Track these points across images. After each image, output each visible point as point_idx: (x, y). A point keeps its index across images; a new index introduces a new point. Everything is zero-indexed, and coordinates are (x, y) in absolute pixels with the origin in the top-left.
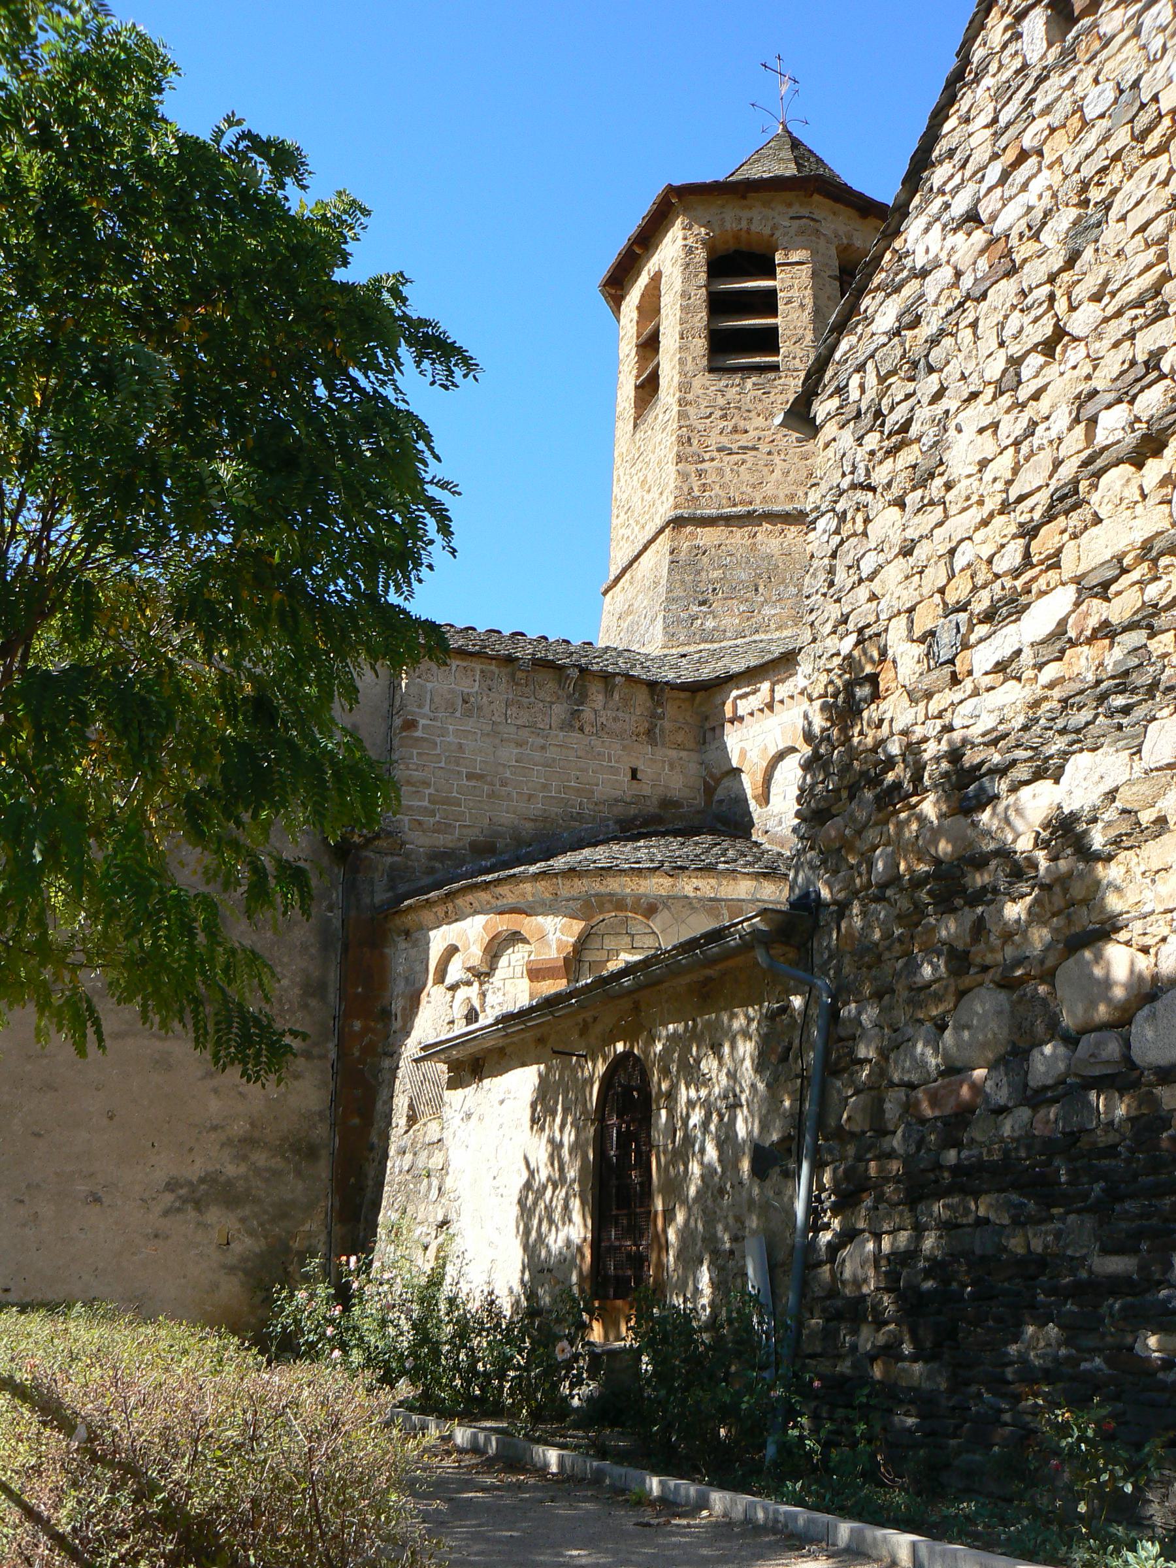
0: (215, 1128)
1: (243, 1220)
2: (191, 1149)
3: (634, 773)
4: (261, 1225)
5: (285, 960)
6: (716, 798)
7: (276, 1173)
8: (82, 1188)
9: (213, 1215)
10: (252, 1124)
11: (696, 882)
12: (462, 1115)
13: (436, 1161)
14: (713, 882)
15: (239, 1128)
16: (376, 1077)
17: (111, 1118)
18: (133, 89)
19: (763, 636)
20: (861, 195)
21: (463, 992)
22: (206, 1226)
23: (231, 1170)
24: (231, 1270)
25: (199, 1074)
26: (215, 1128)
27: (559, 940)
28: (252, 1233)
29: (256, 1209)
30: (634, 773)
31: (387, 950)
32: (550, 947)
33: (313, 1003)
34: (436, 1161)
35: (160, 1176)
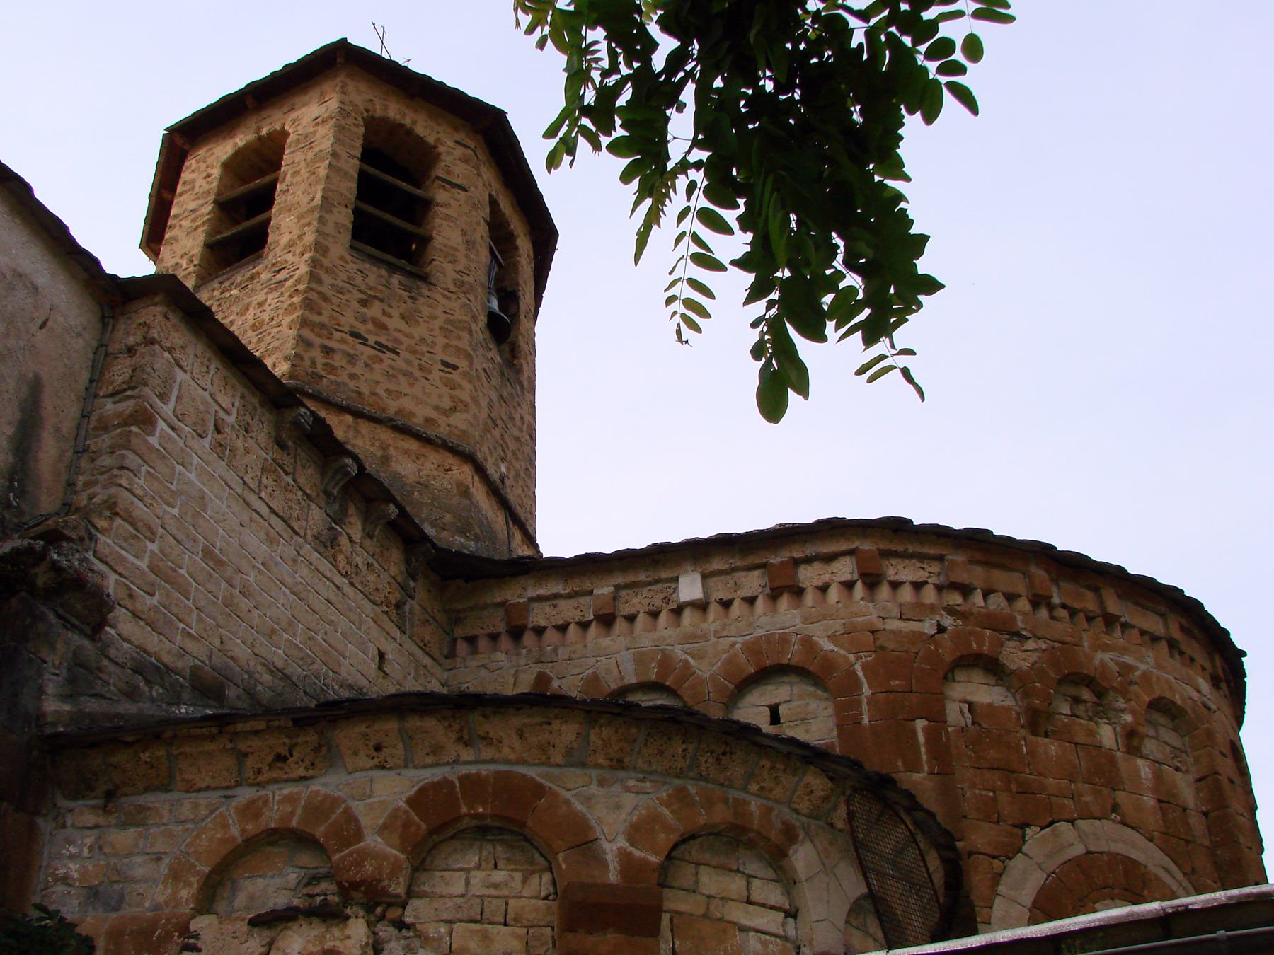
31: (40, 821)
32: (604, 865)
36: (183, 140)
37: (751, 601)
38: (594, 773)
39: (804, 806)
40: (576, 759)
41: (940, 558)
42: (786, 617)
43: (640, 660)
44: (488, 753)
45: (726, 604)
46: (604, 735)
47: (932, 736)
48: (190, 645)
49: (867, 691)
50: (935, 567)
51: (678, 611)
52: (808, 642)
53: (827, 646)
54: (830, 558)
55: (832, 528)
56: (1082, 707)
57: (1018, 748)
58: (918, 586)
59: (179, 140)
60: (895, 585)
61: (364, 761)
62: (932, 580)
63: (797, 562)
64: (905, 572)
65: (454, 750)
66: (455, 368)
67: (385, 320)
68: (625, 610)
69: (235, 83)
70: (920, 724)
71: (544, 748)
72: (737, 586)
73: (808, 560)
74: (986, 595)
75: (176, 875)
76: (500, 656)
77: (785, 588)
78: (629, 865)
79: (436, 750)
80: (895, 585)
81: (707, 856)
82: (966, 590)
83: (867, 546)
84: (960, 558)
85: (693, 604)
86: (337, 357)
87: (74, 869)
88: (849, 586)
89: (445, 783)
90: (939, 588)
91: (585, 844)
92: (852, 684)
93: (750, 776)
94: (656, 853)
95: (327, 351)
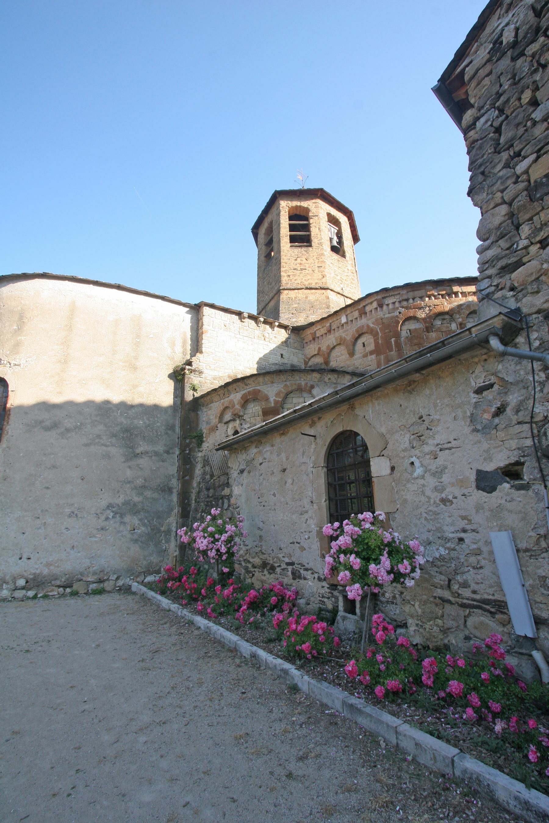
0: (129, 482)
1: (140, 520)
2: (118, 492)
3: (282, 355)
4: (149, 521)
5: (159, 415)
6: (308, 365)
7: (154, 499)
8: (68, 510)
9: (127, 518)
10: (145, 480)
11: (329, 376)
12: (238, 471)
13: (226, 491)
14: (336, 376)
15: (139, 482)
16: (195, 460)
17: (82, 479)
18: (145, 595)
19: (480, 161)
20: (333, 198)
21: (231, 425)
22: (125, 523)
23: (136, 499)
24: (136, 541)
25: (123, 460)
26: (129, 482)
27: (274, 400)
28: (144, 525)
29: (146, 515)
30: (282, 355)
31: (199, 412)
32: (271, 403)
33: (170, 432)
34: (226, 491)
35: (104, 503)
36: (255, 230)
37: (357, 318)
38: (269, 385)
39: (316, 380)
40: (265, 384)
41: (399, 294)
42: (364, 321)
43: (336, 339)
44: (250, 386)
45: (352, 321)
46: (267, 378)
47: (396, 342)
48: (226, 371)
49: (380, 334)
50: (398, 297)
51: (343, 325)
52: (368, 326)
53: (372, 325)
54: (371, 303)
55: (369, 296)
56: (445, 321)
57: (423, 338)
58: (394, 303)
59: (254, 231)
60: (388, 305)
61: (235, 392)
62: (398, 300)
63: (364, 306)
64: (390, 301)
65: (245, 387)
66: (321, 267)
67: (301, 262)
68: (333, 328)
69: (262, 207)
70: (393, 340)
71: (259, 383)
72: (353, 316)
73: (367, 305)
74: (413, 299)
75: (216, 418)
76: (312, 345)
77: (363, 313)
78: (276, 402)
79: (243, 388)
80: (388, 305)
81: (295, 396)
82: (407, 300)
83: (379, 297)
84: (404, 292)
85: (345, 323)
86: (291, 277)
87: (204, 419)
88: (376, 309)
89: (246, 393)
90: (400, 302)
91: (267, 399)
92: (377, 333)
93: (300, 378)
94: (280, 398)
95: (289, 276)
